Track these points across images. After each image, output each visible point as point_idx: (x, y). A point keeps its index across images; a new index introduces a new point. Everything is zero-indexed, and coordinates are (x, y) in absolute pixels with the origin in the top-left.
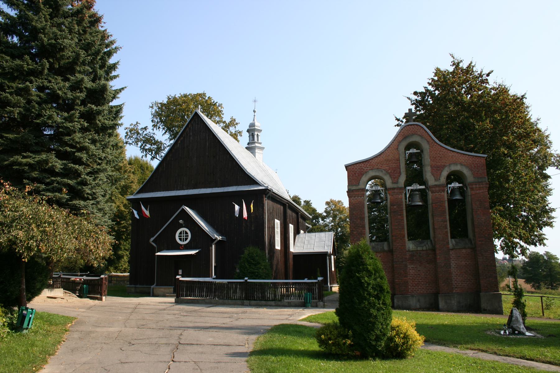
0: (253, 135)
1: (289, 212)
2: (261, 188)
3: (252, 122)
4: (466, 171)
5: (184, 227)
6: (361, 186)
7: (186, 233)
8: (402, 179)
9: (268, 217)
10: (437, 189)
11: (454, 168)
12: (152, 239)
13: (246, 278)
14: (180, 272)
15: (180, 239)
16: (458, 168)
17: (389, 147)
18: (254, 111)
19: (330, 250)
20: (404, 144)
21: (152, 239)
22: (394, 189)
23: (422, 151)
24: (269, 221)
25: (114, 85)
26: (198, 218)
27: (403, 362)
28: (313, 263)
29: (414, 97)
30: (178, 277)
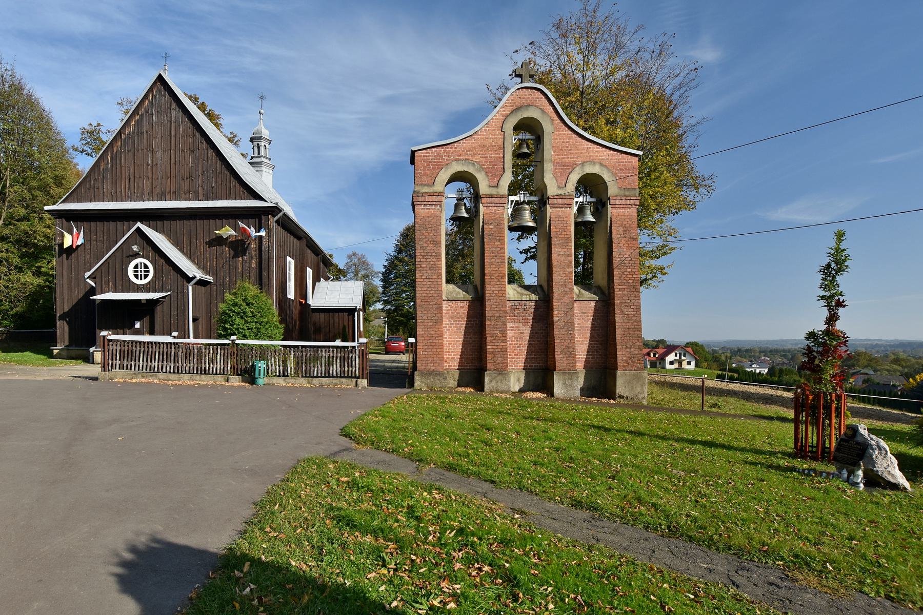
10: (560, 201)
11: (589, 169)
12: (87, 274)
13: (233, 338)
15: (136, 276)
21: (87, 274)
22: (491, 196)
24: (278, 258)
29: (128, 556)
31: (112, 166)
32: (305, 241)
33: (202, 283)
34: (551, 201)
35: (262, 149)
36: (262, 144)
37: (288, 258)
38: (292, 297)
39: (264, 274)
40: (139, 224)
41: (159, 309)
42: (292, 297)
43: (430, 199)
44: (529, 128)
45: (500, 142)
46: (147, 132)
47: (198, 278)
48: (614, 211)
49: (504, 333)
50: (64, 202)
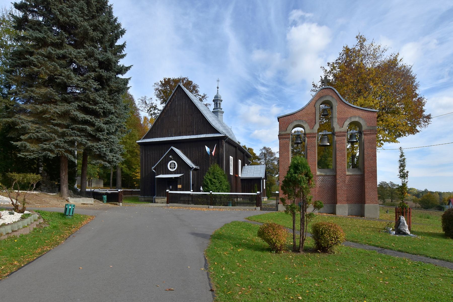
0: (217, 104)
1: (239, 152)
2: (221, 135)
3: (216, 94)
4: (362, 122)
6: (288, 132)
7: (174, 164)
8: (317, 127)
9: (226, 154)
11: (353, 120)
12: (153, 168)
13: (211, 192)
14: (171, 187)
15: (171, 168)
16: (357, 119)
17: (309, 104)
18: (218, 88)
19: (262, 175)
20: (320, 102)
21: (153, 168)
23: (332, 108)
25: (122, 62)
26: (180, 154)
27: (325, 255)
28: (251, 184)
30: (167, 191)
33: (195, 169)
34: (336, 134)
37: (230, 157)
38: (232, 174)
40: (172, 147)
42: (232, 174)
43: (285, 136)
45: (314, 112)
48: (366, 136)
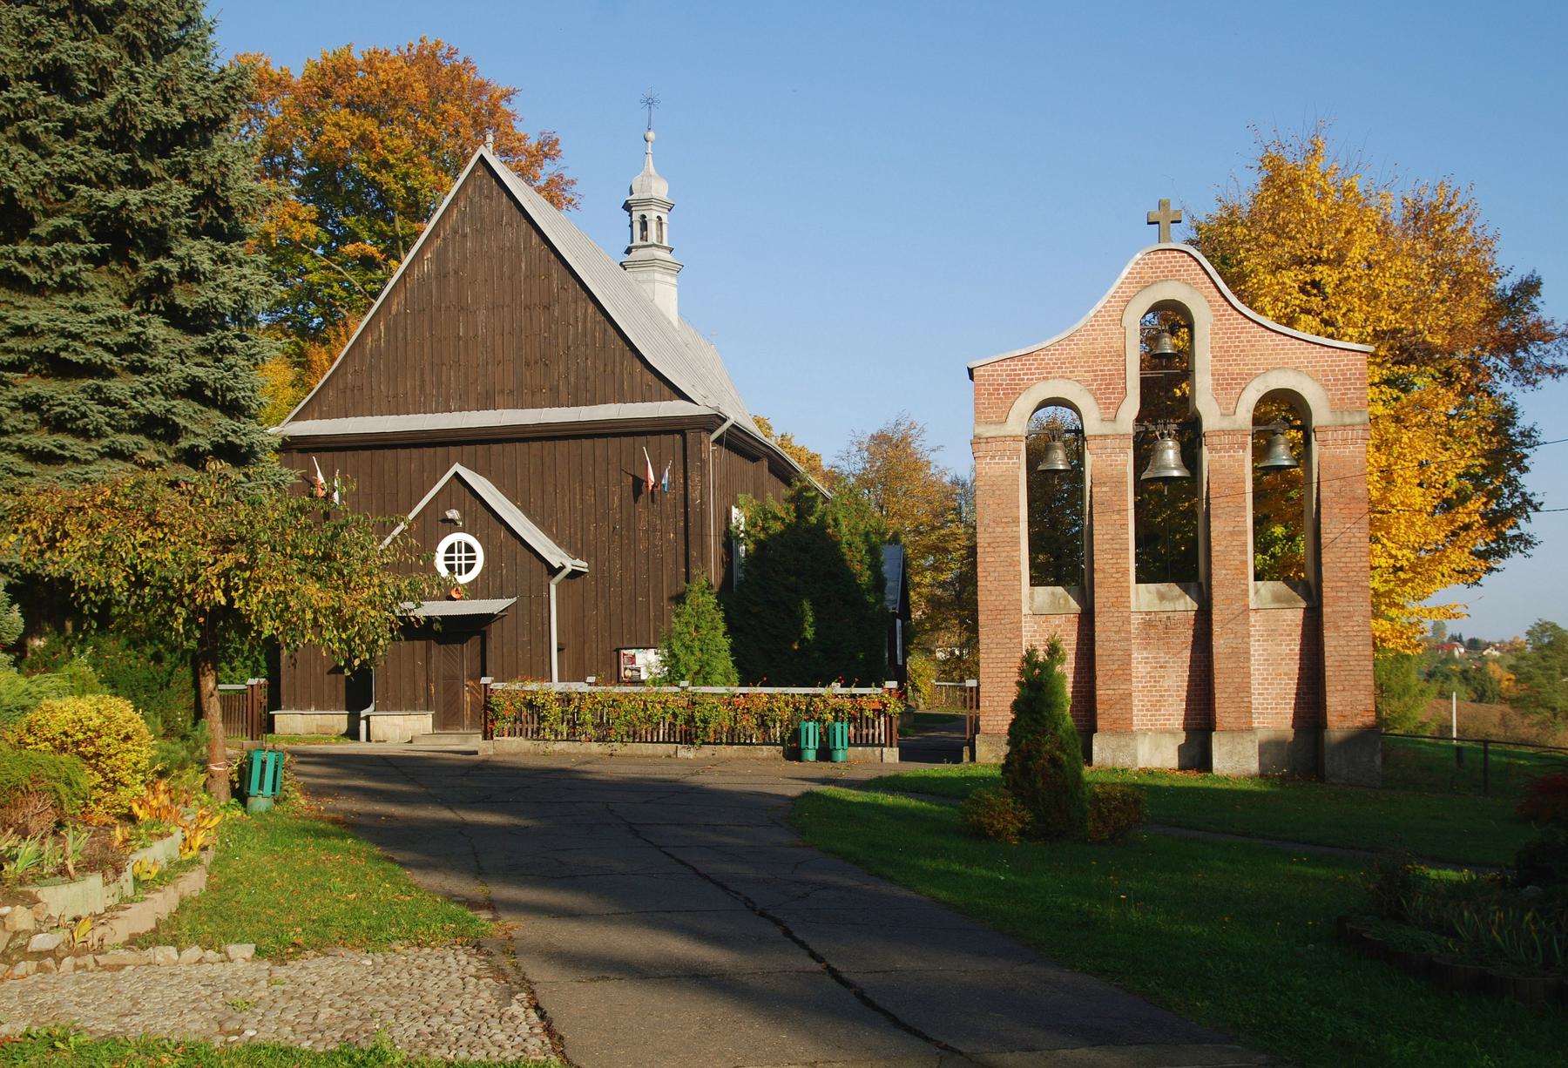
5: (463, 530)
13: (683, 684)
31: (388, 342)
32: (766, 463)
34: (1208, 440)
35: (652, 226)
36: (652, 216)
39: (694, 553)
40: (457, 468)
41: (494, 628)
44: (1173, 316)
46: (456, 272)
47: (569, 569)
49: (1126, 664)
50: (295, 419)
